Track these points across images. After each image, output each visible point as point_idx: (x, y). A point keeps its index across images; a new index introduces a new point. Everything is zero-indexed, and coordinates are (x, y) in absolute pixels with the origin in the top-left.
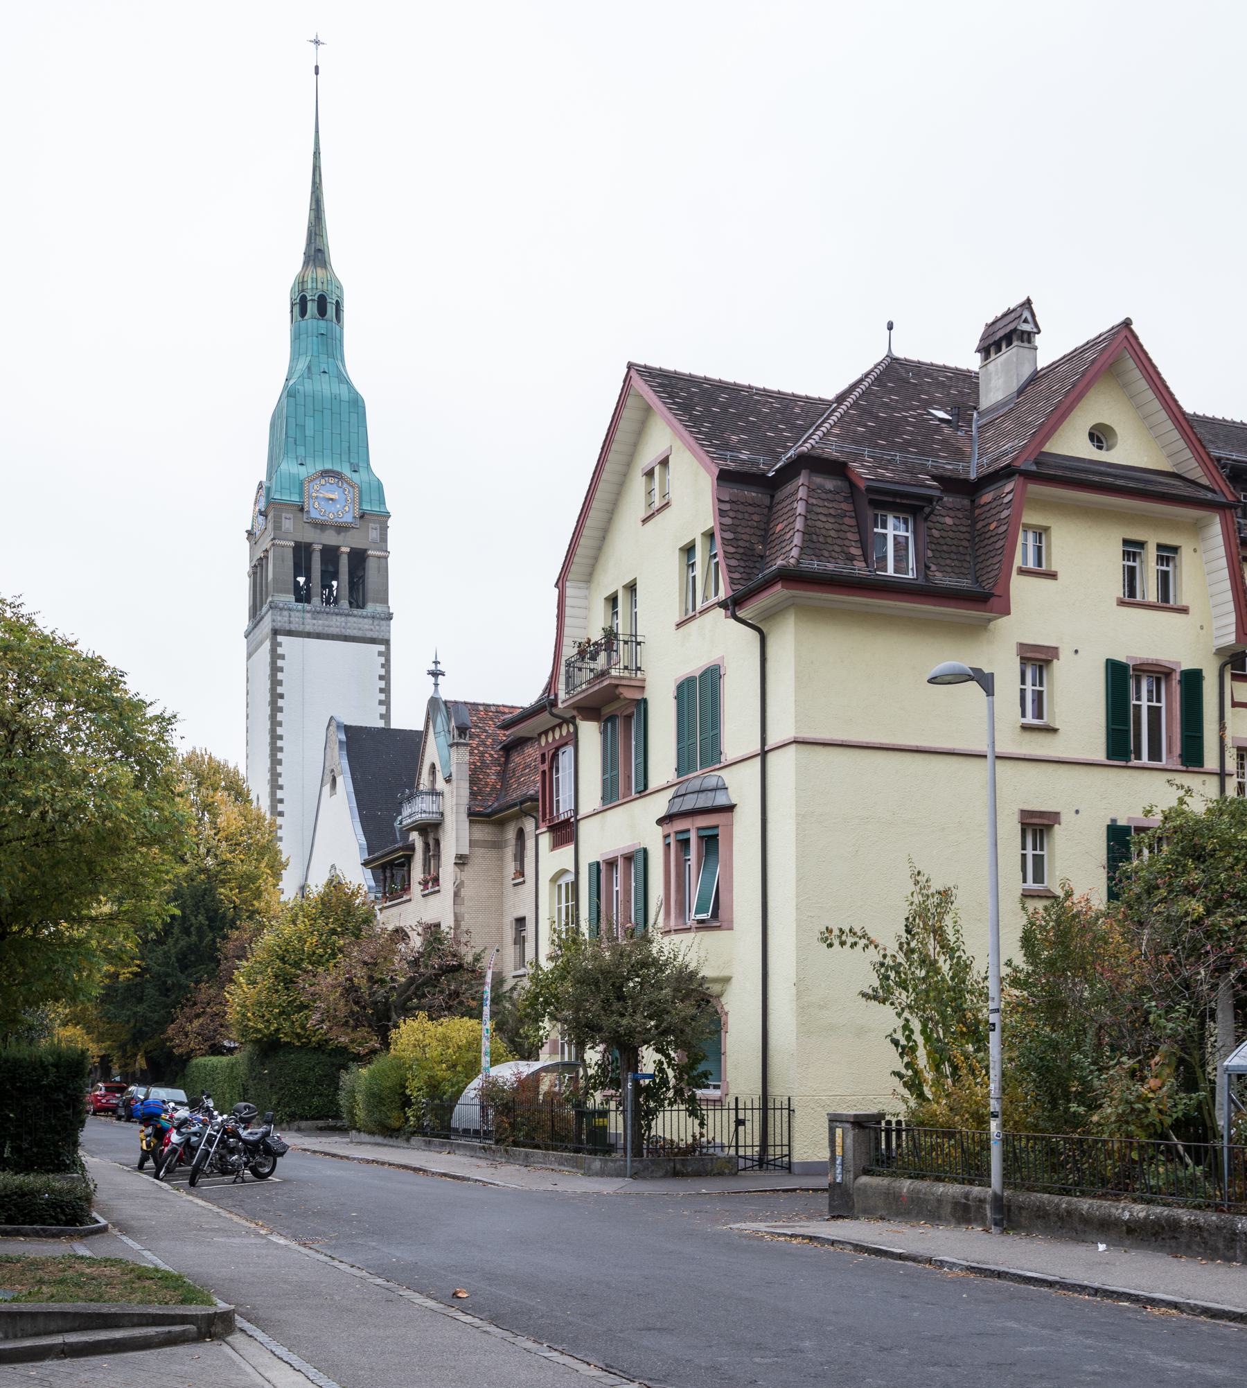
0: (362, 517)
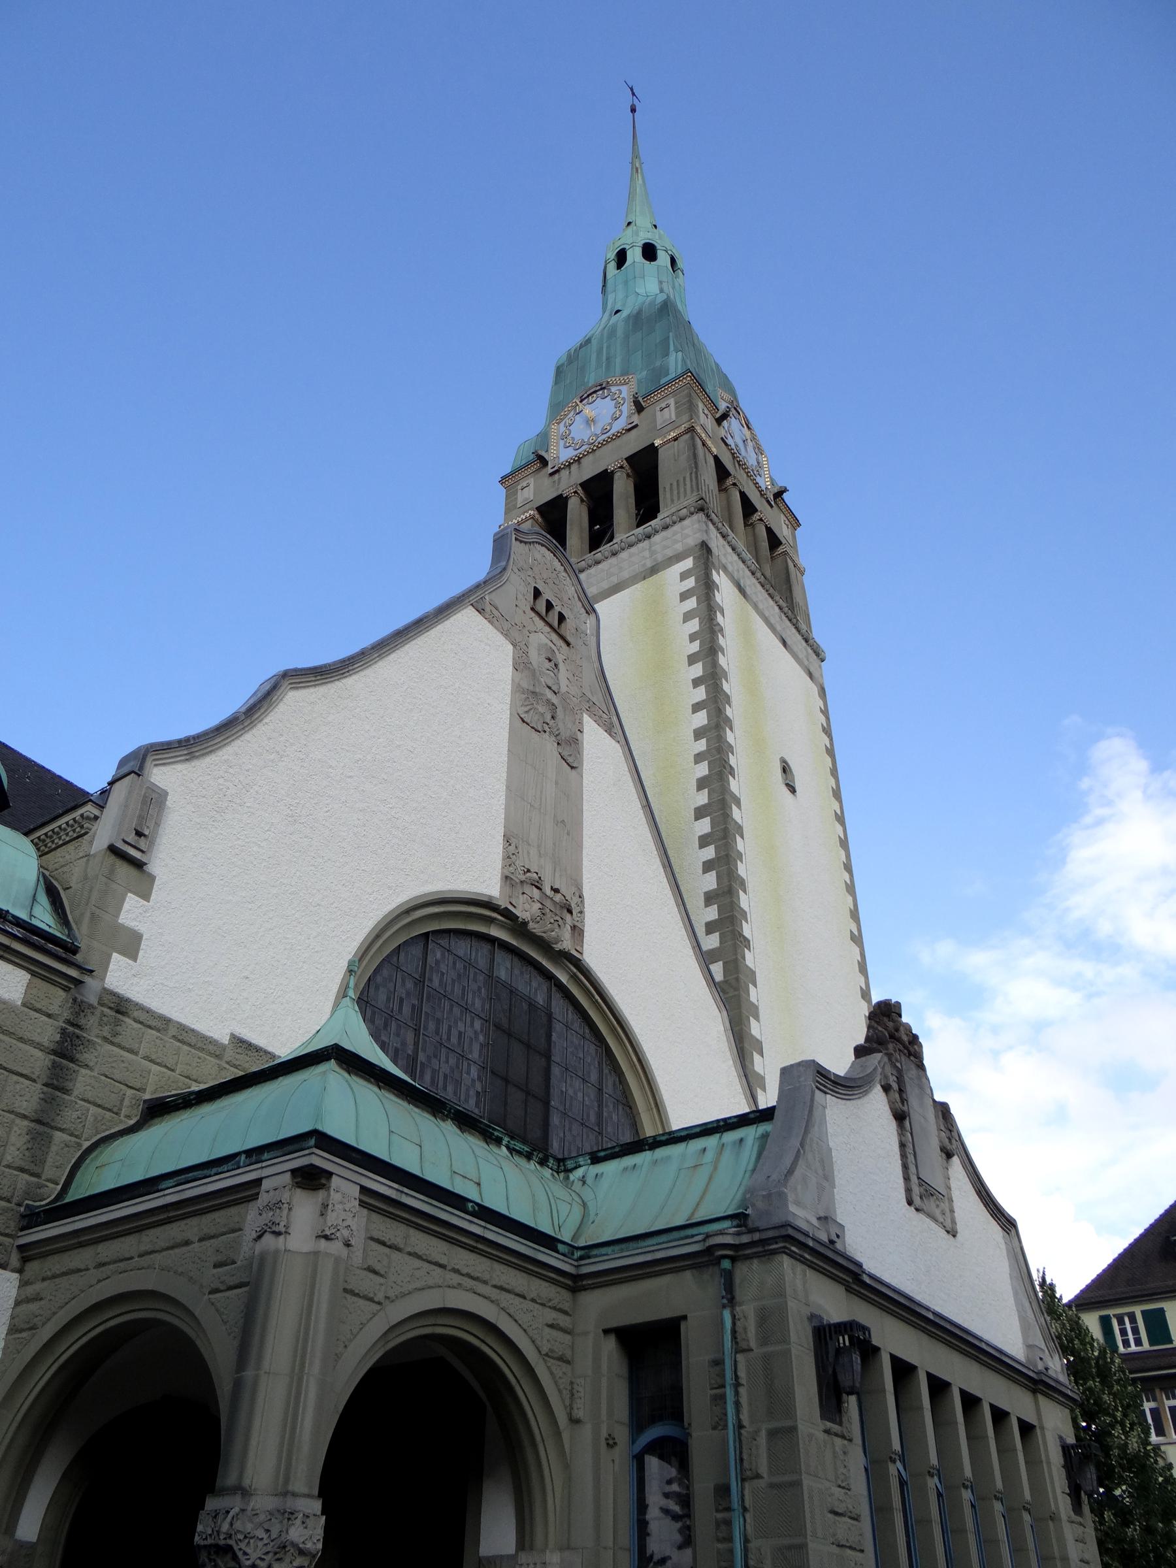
0: (639, 408)
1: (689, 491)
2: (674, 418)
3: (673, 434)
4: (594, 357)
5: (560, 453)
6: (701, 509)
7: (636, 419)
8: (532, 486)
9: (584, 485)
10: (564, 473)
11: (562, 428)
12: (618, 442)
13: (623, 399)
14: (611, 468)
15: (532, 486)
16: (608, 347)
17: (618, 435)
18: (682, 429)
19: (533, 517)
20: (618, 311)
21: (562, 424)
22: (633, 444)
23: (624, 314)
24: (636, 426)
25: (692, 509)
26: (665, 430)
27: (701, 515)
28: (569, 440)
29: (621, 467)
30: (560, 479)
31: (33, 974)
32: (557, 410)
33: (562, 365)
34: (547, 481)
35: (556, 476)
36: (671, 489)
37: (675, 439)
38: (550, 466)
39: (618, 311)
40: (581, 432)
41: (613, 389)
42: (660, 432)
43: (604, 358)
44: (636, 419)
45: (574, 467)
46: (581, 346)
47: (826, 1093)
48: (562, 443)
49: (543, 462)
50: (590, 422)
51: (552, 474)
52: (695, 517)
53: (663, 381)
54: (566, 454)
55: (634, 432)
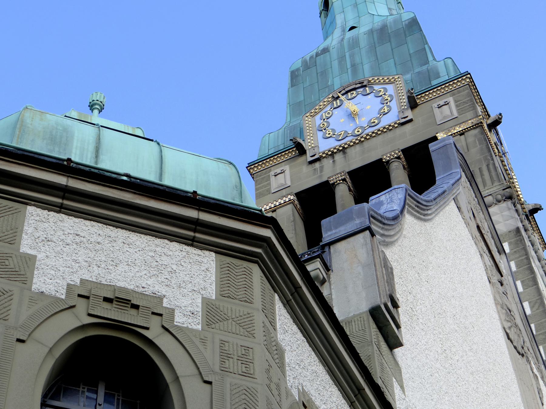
0: (413, 104)
1: (488, 182)
2: (456, 114)
3: (458, 129)
4: (335, 64)
5: (318, 143)
6: (510, 198)
7: (410, 114)
8: (287, 172)
9: (351, 174)
10: (327, 163)
11: (318, 120)
12: (390, 135)
13: (390, 96)
14: (386, 158)
15: (287, 172)
16: (352, 56)
17: (389, 129)
18: (470, 124)
19: (291, 202)
20: (352, 28)
21: (318, 117)
22: (410, 137)
23: (363, 29)
24: (411, 121)
25: (499, 197)
26: (446, 125)
27: (509, 203)
28: (329, 131)
29: (399, 158)
30: (322, 168)
31: (216, 252)
32: (299, 108)
33: (298, 70)
34: (306, 169)
35: (317, 165)
36: (6, 307)
37: (462, 133)
38: (309, 154)
39: (352, 28)
40: (339, 122)
41: (376, 87)
42: (442, 126)
43: (349, 66)
44: (410, 114)
45: (338, 157)
46: (317, 55)
47: (275, 291)
48: (320, 134)
49: (301, 150)
50: (352, 116)
51: (311, 162)
52: (504, 205)
53: (434, 82)
54: (325, 145)
55: (408, 126)
